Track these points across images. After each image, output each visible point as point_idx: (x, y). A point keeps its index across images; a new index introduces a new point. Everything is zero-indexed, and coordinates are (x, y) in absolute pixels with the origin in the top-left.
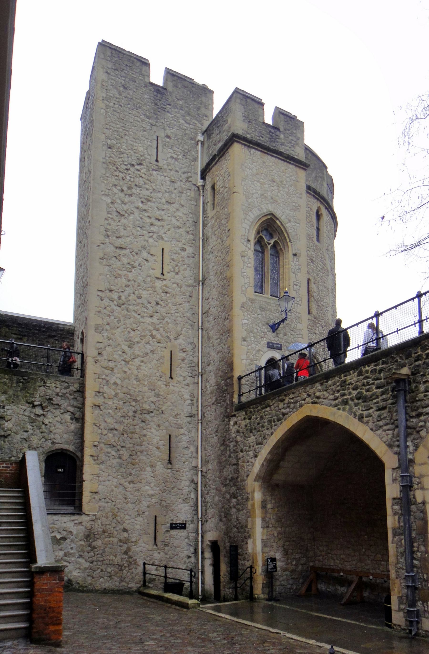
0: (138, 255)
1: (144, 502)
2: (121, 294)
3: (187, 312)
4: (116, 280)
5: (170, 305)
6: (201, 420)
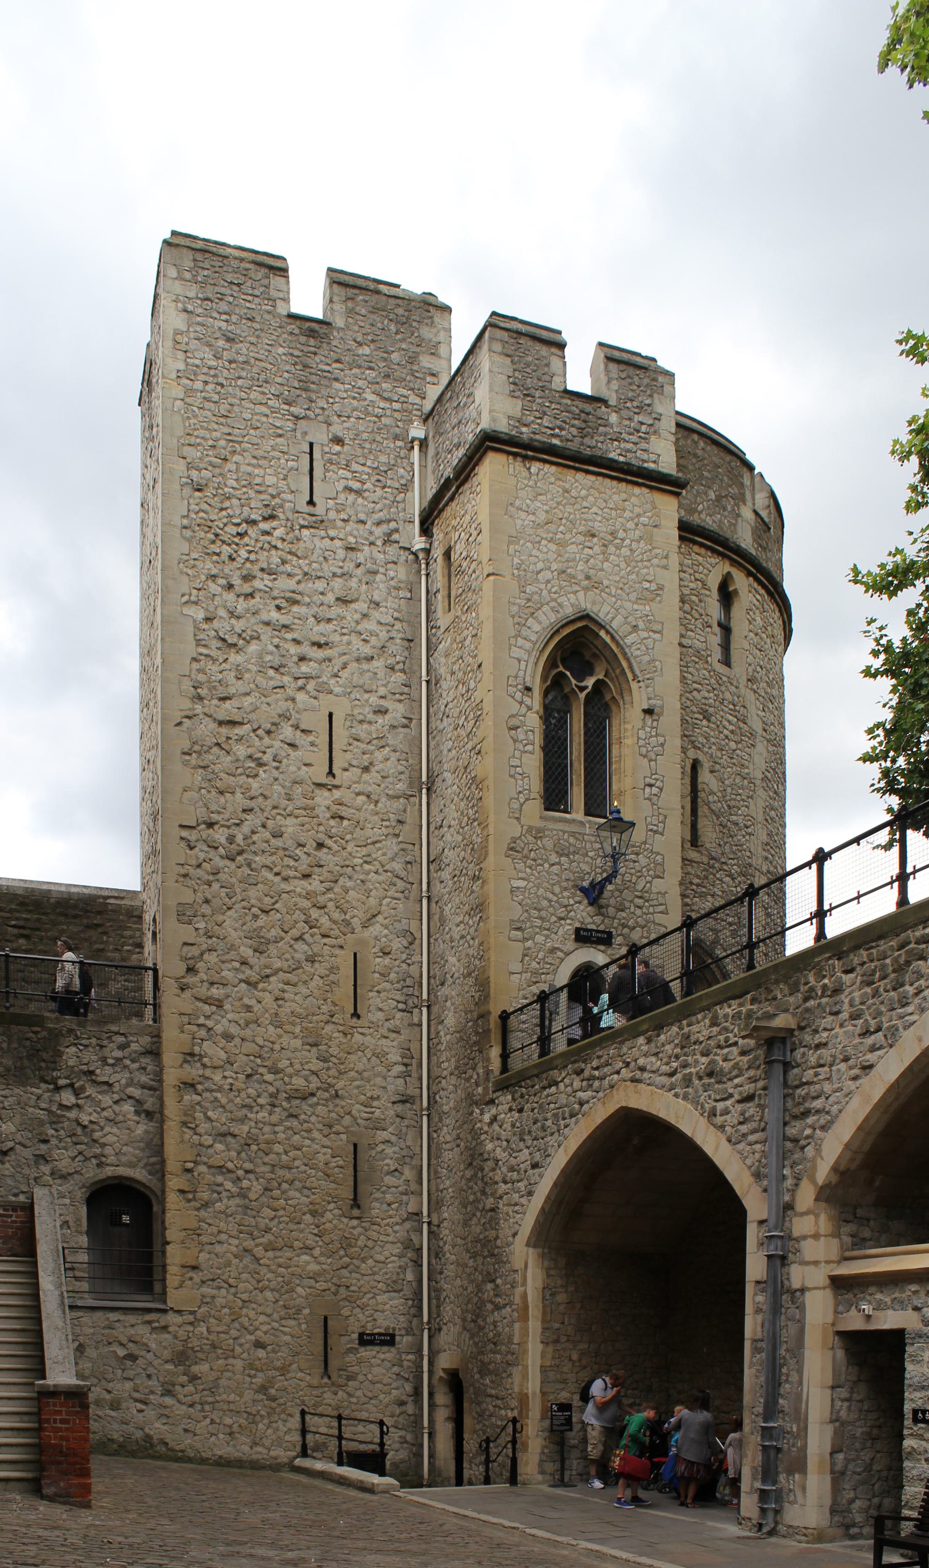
0: (273, 735)
1: (299, 1289)
2: (234, 831)
3: (393, 859)
4: (222, 800)
5: (350, 847)
6: (428, 1109)
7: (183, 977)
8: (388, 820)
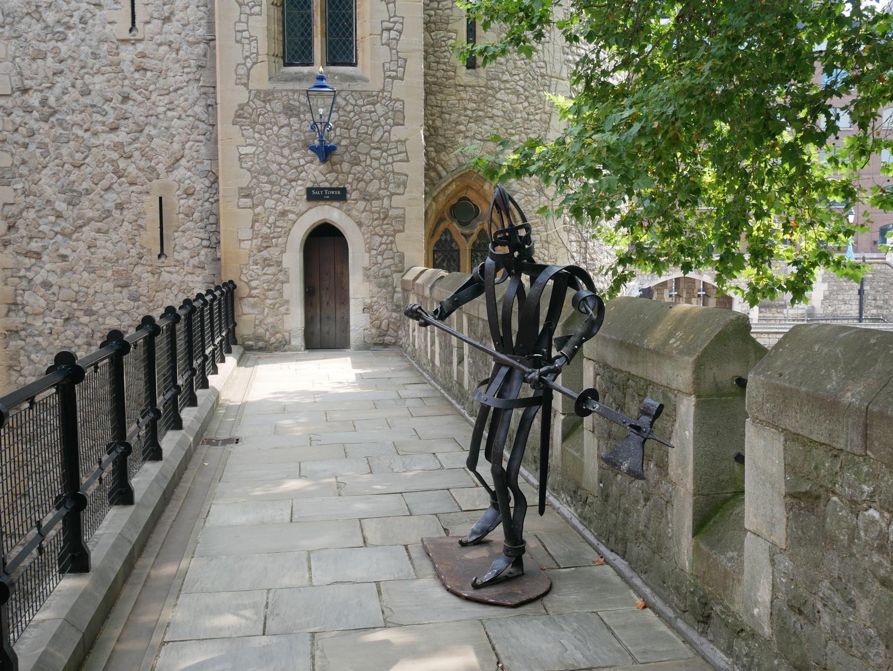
2: (47, 93)
5: (154, 97)
7: (5, 235)
8: (189, 66)
